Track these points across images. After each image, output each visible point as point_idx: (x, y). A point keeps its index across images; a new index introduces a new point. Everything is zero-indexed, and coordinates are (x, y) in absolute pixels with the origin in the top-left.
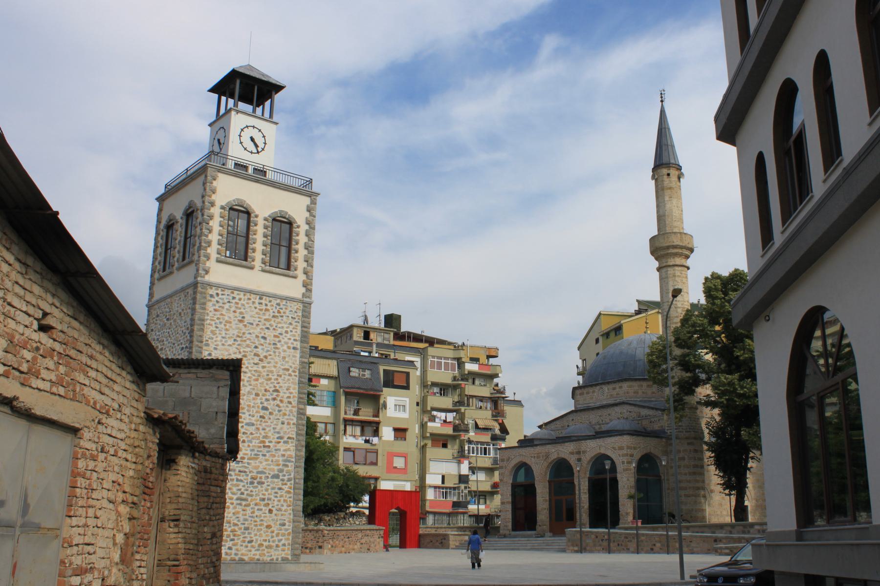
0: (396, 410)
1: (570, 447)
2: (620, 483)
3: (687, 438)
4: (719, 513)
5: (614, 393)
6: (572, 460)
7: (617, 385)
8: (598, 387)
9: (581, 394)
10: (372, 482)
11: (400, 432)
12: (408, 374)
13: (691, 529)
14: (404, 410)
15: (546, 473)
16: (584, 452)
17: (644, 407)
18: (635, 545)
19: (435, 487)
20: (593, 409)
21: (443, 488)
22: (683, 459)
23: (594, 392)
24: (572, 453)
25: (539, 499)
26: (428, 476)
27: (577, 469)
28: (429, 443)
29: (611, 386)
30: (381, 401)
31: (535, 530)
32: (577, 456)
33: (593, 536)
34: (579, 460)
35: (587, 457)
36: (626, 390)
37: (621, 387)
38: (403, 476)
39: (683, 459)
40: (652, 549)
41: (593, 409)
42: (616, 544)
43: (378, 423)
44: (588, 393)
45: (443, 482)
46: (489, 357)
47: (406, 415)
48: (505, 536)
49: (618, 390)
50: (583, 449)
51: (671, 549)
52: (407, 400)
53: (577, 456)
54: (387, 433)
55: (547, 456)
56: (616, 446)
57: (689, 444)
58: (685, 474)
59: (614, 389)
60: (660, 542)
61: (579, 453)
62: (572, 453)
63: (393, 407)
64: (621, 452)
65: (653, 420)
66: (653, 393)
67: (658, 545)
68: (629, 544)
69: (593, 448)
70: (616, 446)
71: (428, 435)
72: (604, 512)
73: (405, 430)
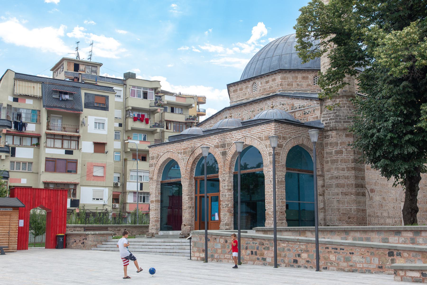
0: (96, 127)
1: (215, 140)
2: (266, 178)
3: (345, 129)
4: (379, 214)
5: (267, 86)
6: (217, 154)
7: (270, 79)
8: (251, 83)
9: (235, 91)
10: (72, 187)
11: (100, 147)
12: (107, 97)
13: (352, 234)
14: (103, 128)
15: (192, 170)
16: (230, 144)
17: (298, 98)
18: (273, 255)
19: (135, 193)
20: (245, 104)
21: (141, 193)
22: (341, 152)
23: (246, 88)
24: (217, 147)
25: (185, 198)
26: (128, 183)
27: (220, 165)
28: (130, 157)
29: (264, 80)
30: (81, 119)
31: (180, 230)
32: (221, 150)
33: (222, 241)
34: (224, 154)
35: (231, 152)
36: (276, 83)
37: (274, 80)
38: (99, 183)
39: (341, 152)
40: (296, 261)
41: (245, 104)
42: (249, 252)
43: (79, 137)
44: (241, 89)
45: (141, 189)
46: (198, 103)
47: (104, 132)
48: (153, 236)
49: (271, 83)
50: (228, 140)
51: (322, 263)
52: (106, 119)
53: (221, 150)
54: (87, 147)
55: (193, 152)
56: (263, 136)
57: (347, 136)
58: (343, 170)
59: (267, 82)
60: (307, 251)
61: (223, 146)
62: (217, 147)
63: (93, 125)
64: (268, 142)
65: (307, 111)
66: (309, 85)
67: (304, 256)
68: (266, 252)
69: (237, 139)
70: (263, 136)
71: (129, 150)
72: (250, 211)
73: (103, 145)
